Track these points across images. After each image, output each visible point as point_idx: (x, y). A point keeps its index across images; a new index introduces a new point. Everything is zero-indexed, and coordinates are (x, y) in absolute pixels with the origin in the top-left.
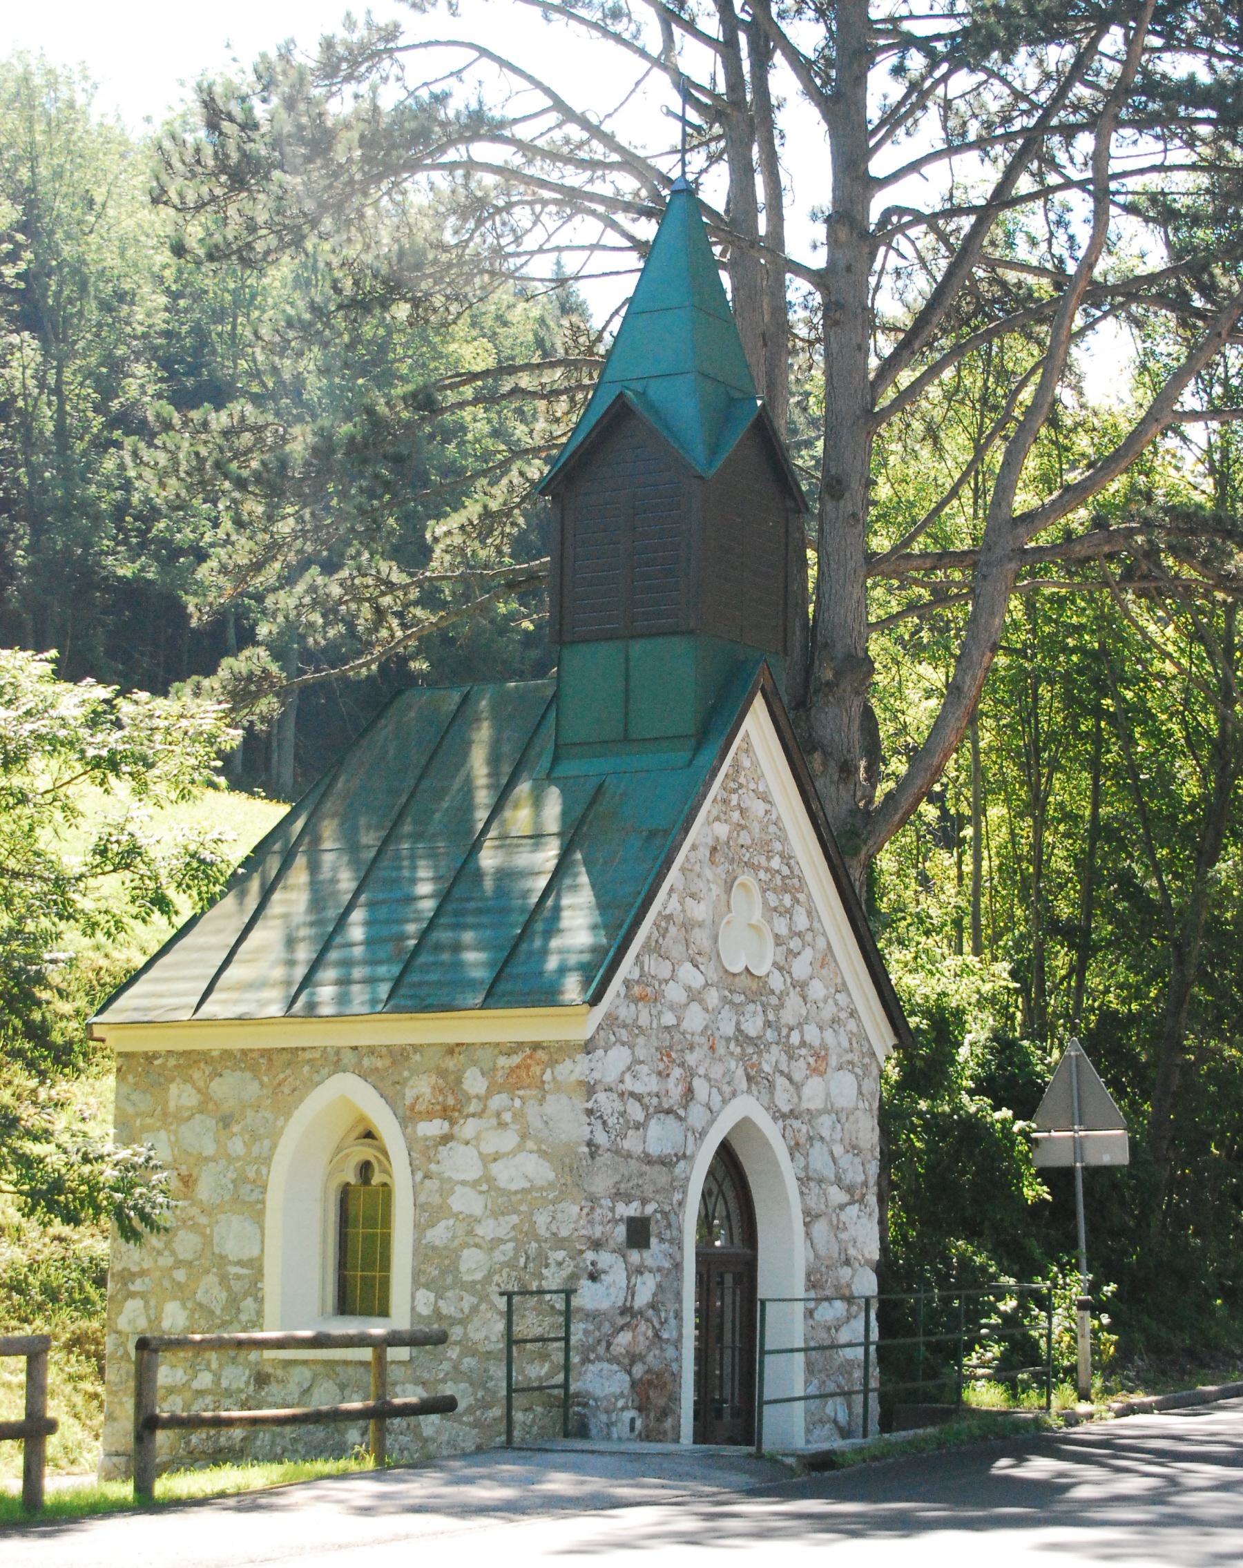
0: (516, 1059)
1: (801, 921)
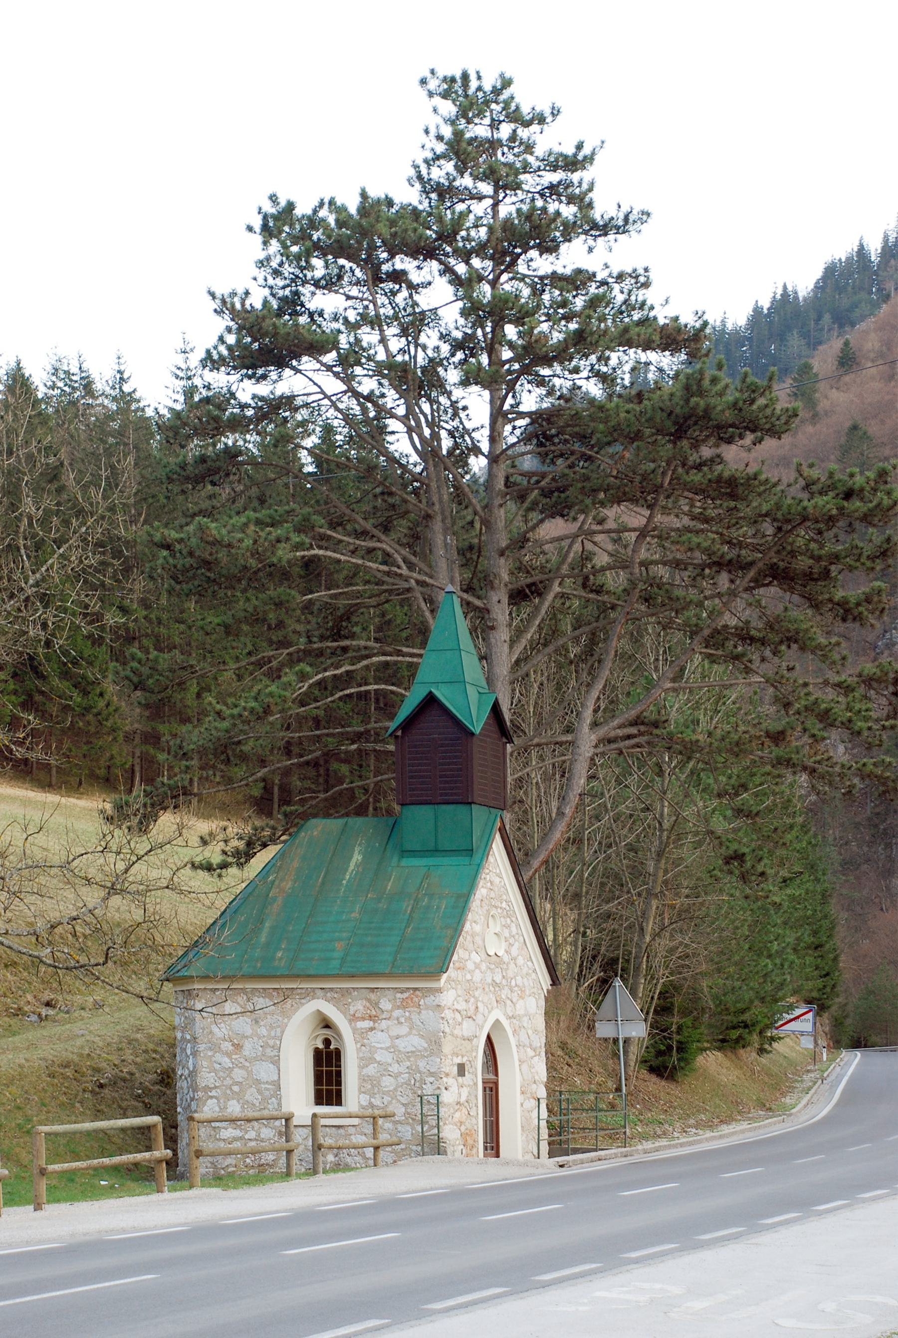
0: (406, 995)
1: (514, 930)
